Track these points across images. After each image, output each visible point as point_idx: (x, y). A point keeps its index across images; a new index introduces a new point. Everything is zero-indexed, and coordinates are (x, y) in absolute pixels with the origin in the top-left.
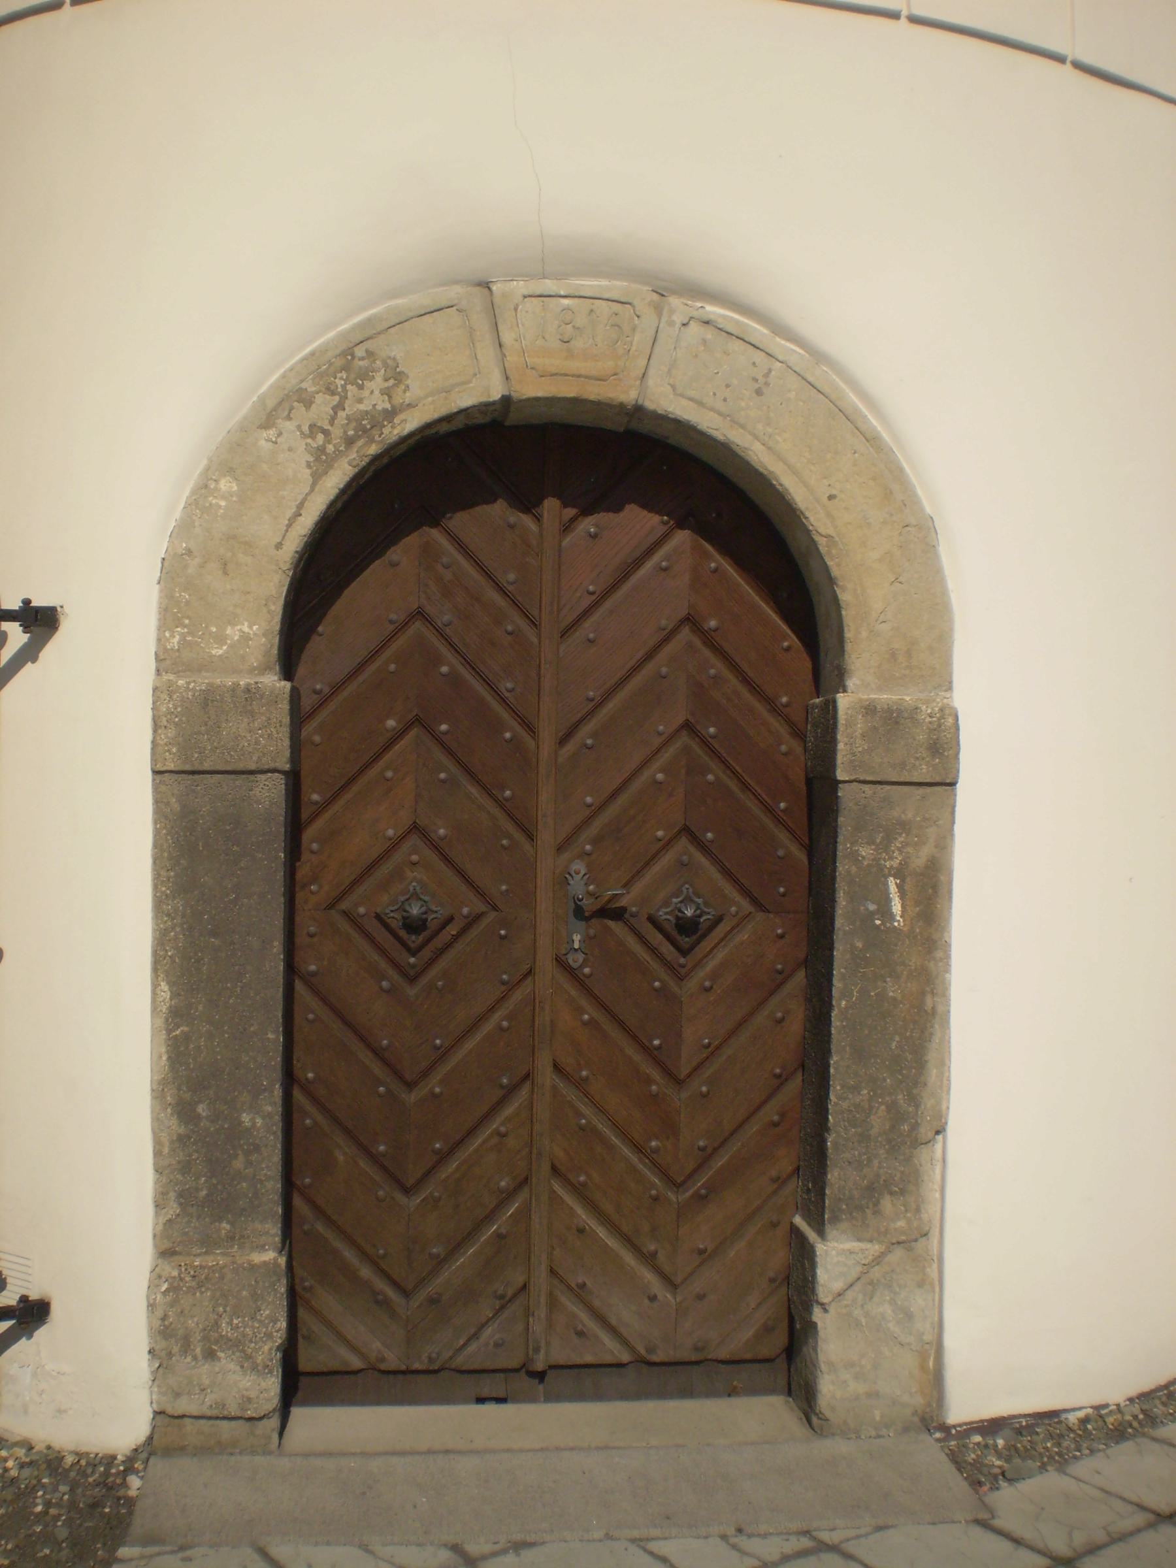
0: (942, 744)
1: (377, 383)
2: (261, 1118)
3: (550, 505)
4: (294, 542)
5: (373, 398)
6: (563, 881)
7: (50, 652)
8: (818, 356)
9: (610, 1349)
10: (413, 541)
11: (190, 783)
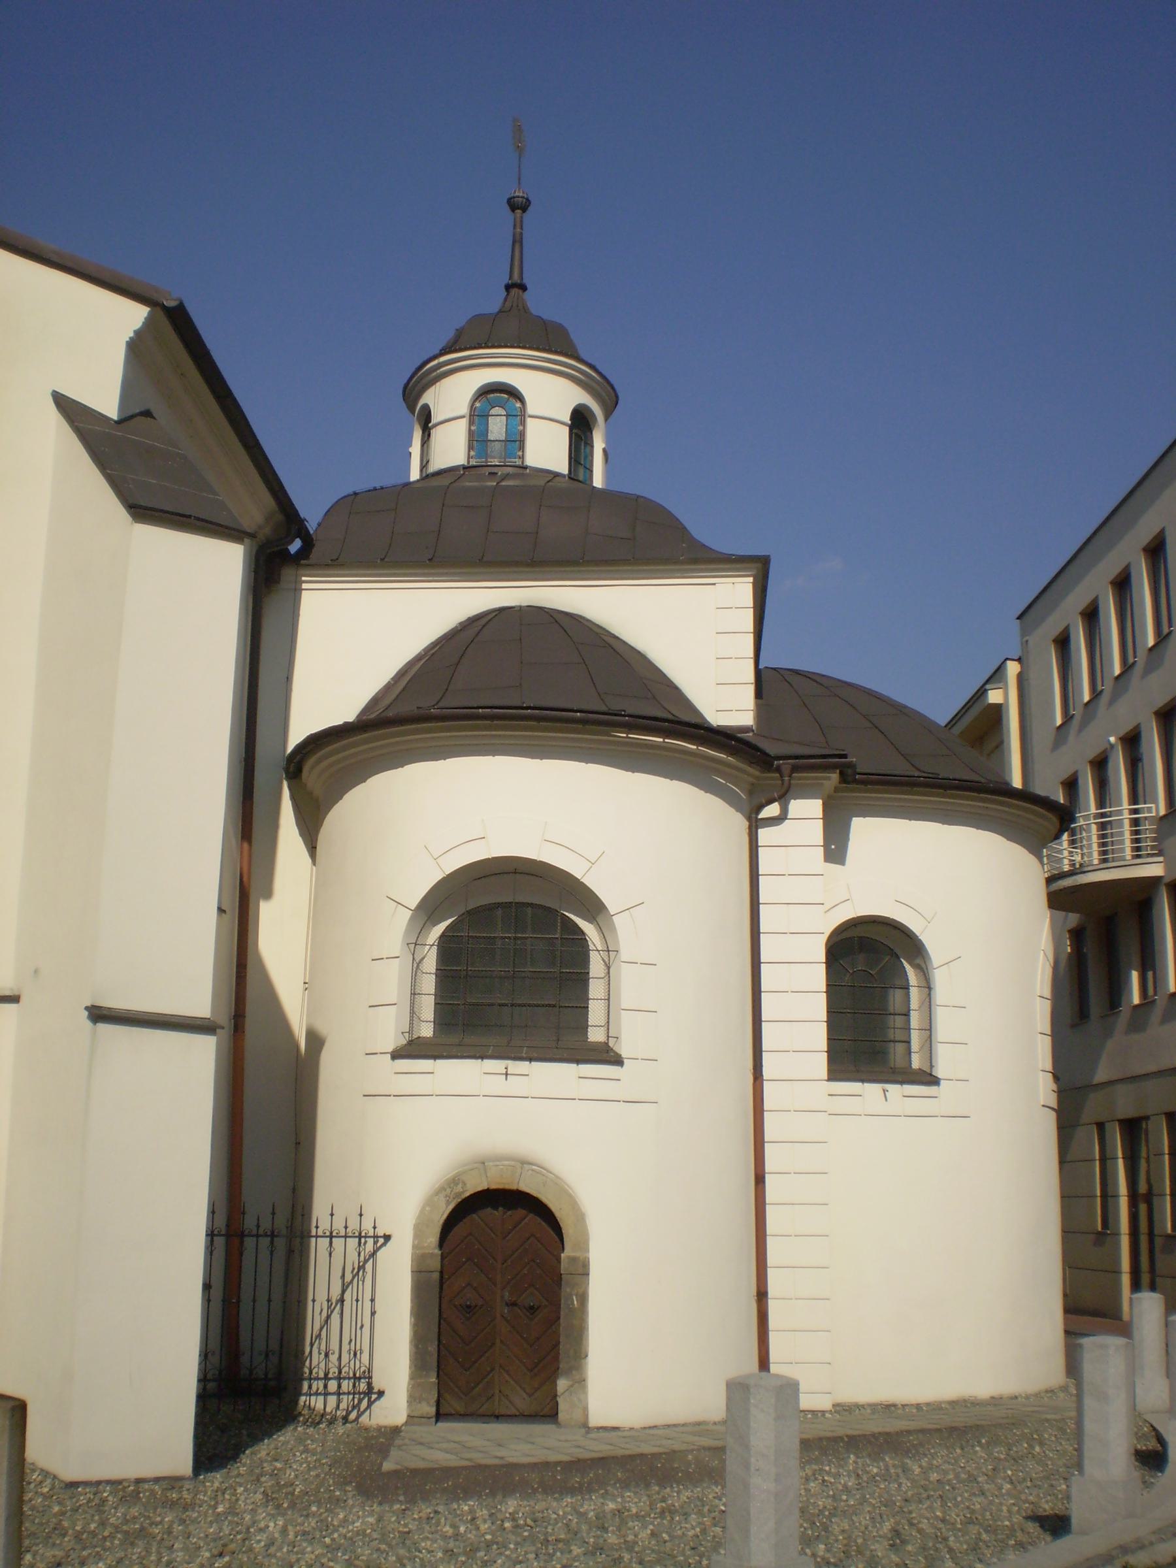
0: (585, 1265)
1: (460, 1186)
2: (433, 1348)
3: (501, 1209)
4: (442, 1221)
5: (459, 1188)
6: (502, 1297)
7: (389, 1244)
8: (557, 1177)
9: (513, 1411)
10: (469, 1218)
11: (419, 1273)
